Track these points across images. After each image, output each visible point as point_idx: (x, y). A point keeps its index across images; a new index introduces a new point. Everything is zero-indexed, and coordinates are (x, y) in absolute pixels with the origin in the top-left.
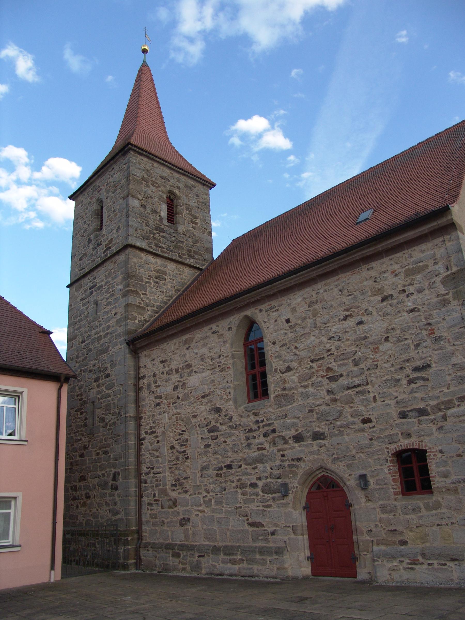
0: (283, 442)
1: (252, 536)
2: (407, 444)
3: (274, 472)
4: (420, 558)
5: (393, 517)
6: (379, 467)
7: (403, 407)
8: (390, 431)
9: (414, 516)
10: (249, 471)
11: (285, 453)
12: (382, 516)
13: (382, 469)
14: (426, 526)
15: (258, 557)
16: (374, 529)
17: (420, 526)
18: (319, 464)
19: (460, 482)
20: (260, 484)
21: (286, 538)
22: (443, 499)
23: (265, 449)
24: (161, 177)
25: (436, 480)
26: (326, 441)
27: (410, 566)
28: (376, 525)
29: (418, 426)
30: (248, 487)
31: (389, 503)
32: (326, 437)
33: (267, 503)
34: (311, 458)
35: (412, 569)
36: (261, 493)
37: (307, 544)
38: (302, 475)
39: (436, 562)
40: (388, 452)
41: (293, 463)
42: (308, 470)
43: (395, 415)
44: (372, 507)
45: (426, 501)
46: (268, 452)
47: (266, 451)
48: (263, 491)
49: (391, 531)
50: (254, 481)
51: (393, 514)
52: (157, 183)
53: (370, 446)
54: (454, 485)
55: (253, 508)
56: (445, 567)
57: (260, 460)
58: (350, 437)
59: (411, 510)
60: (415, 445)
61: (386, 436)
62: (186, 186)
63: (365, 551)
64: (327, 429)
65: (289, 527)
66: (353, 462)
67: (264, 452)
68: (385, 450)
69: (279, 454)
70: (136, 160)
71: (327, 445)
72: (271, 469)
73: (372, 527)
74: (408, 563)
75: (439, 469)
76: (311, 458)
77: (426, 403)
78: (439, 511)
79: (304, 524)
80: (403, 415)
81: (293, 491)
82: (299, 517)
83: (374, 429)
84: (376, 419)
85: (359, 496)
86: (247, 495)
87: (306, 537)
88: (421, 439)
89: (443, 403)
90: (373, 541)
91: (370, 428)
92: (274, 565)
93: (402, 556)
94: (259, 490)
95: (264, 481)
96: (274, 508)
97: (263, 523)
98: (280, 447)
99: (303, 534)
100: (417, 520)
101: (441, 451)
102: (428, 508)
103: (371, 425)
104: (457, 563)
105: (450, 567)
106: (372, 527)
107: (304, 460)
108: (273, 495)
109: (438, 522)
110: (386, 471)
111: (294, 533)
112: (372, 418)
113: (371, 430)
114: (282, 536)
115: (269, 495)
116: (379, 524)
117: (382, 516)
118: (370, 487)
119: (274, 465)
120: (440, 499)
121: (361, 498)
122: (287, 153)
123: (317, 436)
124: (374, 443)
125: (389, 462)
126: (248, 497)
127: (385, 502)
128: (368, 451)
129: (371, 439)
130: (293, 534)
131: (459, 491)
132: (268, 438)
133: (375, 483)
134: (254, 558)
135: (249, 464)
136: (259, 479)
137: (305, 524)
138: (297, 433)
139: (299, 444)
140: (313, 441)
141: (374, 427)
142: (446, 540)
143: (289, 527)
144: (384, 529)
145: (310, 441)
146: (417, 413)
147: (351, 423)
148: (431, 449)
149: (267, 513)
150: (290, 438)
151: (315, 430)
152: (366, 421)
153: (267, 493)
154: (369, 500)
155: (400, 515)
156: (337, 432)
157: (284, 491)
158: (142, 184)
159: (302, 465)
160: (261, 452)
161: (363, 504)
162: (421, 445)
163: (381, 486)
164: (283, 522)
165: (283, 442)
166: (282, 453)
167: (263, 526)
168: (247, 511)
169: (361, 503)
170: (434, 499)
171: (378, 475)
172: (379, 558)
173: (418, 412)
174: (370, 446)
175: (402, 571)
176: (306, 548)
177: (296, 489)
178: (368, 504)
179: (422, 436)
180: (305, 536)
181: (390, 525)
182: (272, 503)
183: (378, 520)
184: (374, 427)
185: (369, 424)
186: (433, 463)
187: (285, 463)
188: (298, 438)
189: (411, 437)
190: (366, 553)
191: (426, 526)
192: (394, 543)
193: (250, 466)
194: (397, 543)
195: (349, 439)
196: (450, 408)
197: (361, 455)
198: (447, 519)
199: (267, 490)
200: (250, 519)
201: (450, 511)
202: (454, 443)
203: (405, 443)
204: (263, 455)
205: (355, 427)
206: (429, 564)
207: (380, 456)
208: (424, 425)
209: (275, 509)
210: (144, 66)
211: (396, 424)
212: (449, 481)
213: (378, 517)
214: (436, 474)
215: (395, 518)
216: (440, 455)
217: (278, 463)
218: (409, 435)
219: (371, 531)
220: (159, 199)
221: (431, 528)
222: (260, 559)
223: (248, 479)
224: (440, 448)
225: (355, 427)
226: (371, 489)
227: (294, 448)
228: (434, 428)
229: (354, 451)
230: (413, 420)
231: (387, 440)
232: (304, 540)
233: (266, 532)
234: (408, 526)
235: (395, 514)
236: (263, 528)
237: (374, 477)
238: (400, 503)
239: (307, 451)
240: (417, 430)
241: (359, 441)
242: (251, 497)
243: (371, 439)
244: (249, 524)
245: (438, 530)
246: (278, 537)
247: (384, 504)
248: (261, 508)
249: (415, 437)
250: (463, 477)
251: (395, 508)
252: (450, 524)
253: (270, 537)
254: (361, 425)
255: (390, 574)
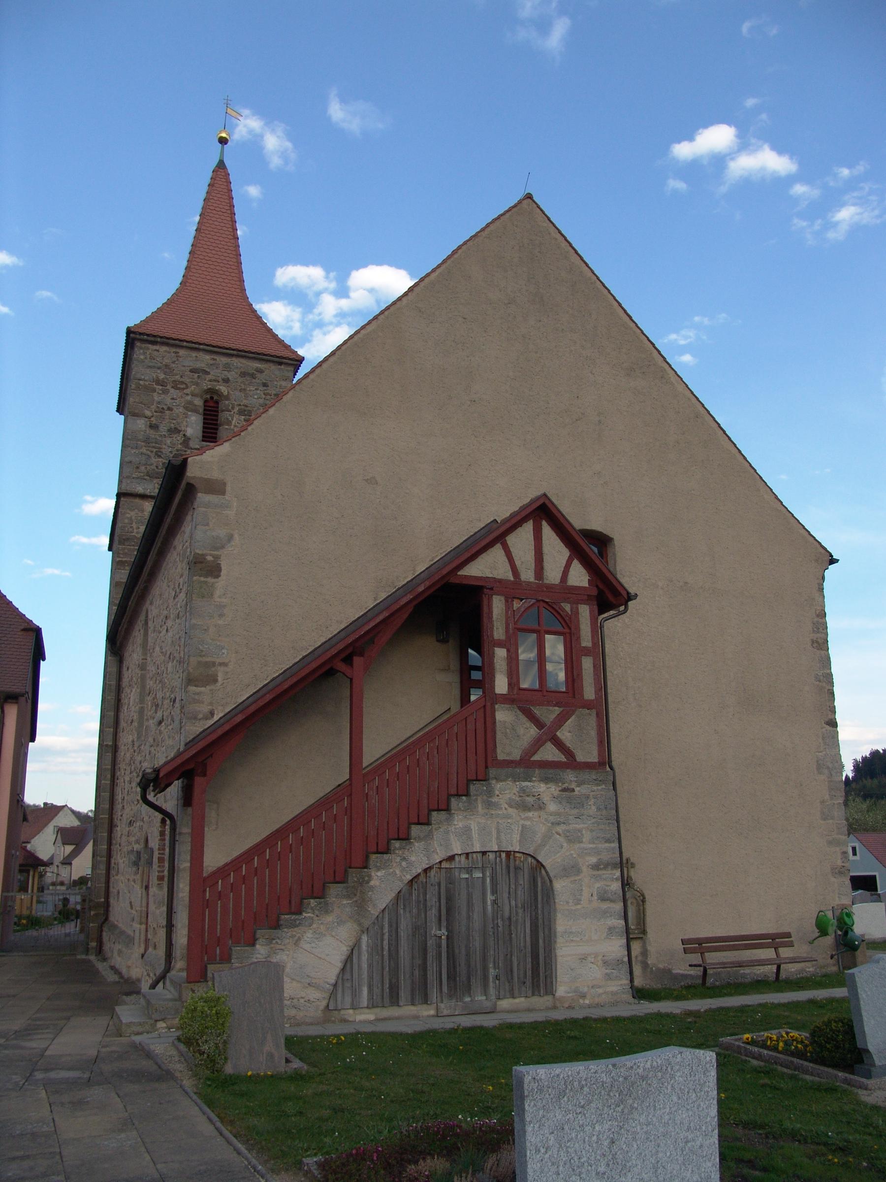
24: (191, 371)
52: (182, 383)
62: (243, 374)
70: (144, 353)
122: (790, 180)
158: (154, 390)
210: (221, 166)
220: (186, 408)
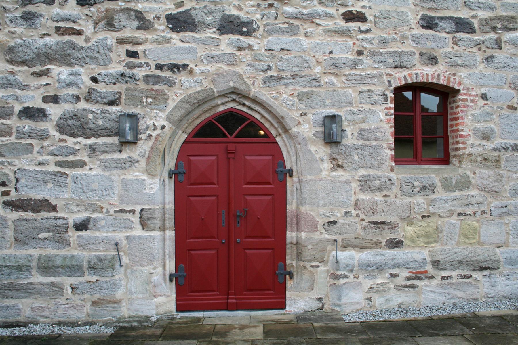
0: (136, 23)
1: (16, 230)
2: (427, 75)
3: (101, 88)
4: (429, 268)
5: (382, 199)
6: (368, 107)
7: (429, 9)
8: (399, 44)
9: (421, 200)
10: (20, 78)
11: (139, 49)
12: (362, 196)
13: (373, 112)
14: (440, 216)
15: (37, 278)
16: (340, 221)
17: (429, 216)
18: (231, 84)
19: (506, 149)
20: (55, 111)
21: (120, 236)
22: (475, 174)
23: (79, 33)
25: (469, 142)
26: (253, 39)
27: (409, 283)
28: (347, 213)
29: (453, 48)
30: (15, 117)
31: (379, 173)
32: (255, 30)
33: (71, 158)
34: (212, 68)
35: (413, 287)
36: (54, 133)
37: (170, 247)
38: (181, 101)
39: (454, 274)
40: (389, 82)
41: (158, 73)
42: (198, 92)
43: (414, 19)
44: (344, 179)
45: (446, 175)
46: (88, 40)
47: (83, 37)
48: (61, 128)
49: (376, 223)
50: (38, 103)
51: (385, 193)
53: (355, 65)
54: (496, 154)
55: (27, 168)
56: (469, 280)
57: (63, 56)
58: (311, 41)
59: (418, 189)
60: (442, 78)
61: (389, 53)
63: (315, 260)
64: (259, 16)
65: (133, 212)
66: (314, 89)
67: (74, 38)
68: (385, 79)
69: (122, 49)
71: (256, 47)
72: (94, 80)
73: (339, 215)
74: (407, 277)
75: (478, 126)
76: (212, 68)
77: (472, 13)
78: (465, 192)
79: (167, 207)
80: (429, 23)
81: (150, 136)
82: (159, 192)
83: (369, 36)
84: (375, 17)
85: (318, 156)
86: (10, 134)
87: (170, 234)
88: (453, 70)
89: (500, 19)
90: (336, 241)
91: (361, 32)
92: (86, 296)
93: (397, 266)
94: (49, 127)
95: (68, 107)
96: (94, 170)
97: (53, 203)
98: (126, 33)
99: (163, 229)
100: (426, 206)
101: (484, 97)
102: (448, 186)
103: (364, 27)
104: (486, 272)
105: (476, 280)
106: (338, 215)
107: (191, 72)
108: (92, 141)
109: (460, 210)
110: (382, 116)
111: (144, 225)
112: (367, 13)
113: (362, 36)
114: (108, 231)
115: (80, 139)
116: (353, 211)
117: (362, 196)
118: (344, 142)
119: (104, 72)
120: (469, 173)
121: (322, 160)
123: (230, 26)
124: (365, 61)
125: (389, 100)
126: (13, 139)
127: (371, 172)
128: (350, 74)
129: (360, 53)
130: (140, 227)
131: (503, 163)
132: (92, 9)
133: (356, 134)
134: (25, 281)
135: (23, 63)
136: (55, 99)
137: (170, 206)
138: (180, 10)
139: (182, 34)
140: (221, 34)
141: (368, 31)
142: (468, 238)
143: (133, 212)
144: (362, 220)
145: (211, 33)
146: (453, 25)
147: (319, 14)
148: (468, 89)
149: (69, 178)
150: (158, 18)
151: (226, 12)
152: (351, 17)
153: (73, 135)
154: (339, 166)
155: (396, 197)
156: (282, 26)
157: (126, 133)
159: (182, 78)
160: (67, 38)
161: (324, 173)
162: (452, 79)
163: (367, 143)
164: (115, 200)
165: (136, 23)
166: (129, 47)
167: (54, 209)
168: (7, 175)
169: (321, 171)
170: (461, 171)
171: (364, 122)
172: (351, 271)
173: (457, 24)
174: (355, 65)
175: (393, 291)
176: (167, 257)
177: (159, 131)
178: (335, 174)
179: (456, 65)
180: (167, 232)
181: (375, 212)
182: (86, 159)
183: (353, 203)
184: (368, 31)
185: (358, 24)
186: (469, 113)
187: (136, 71)
188: (180, 23)
189: (436, 63)
190: (316, 264)
191: (440, 216)
192: (378, 245)
193: (25, 68)
194: (384, 244)
195: (311, 43)
196: (510, 29)
197: (334, 79)
198: (476, 205)
199: (74, 126)
200: (13, 193)
201: (482, 193)
202: (506, 86)
203: (425, 73)
204: (73, 46)
205: (330, 24)
206: (443, 278)
207: (372, 88)
208: (464, 48)
209: (93, 172)
211: (413, 36)
212: (489, 145)
213: (353, 198)
214: (470, 133)
215: (386, 201)
216: (481, 102)
217: (116, 69)
218: (433, 60)
219: (335, 222)
221: (447, 219)
222: (42, 284)
223: (17, 98)
224: (483, 90)
225: (330, 24)
226: (347, 146)
227: (168, 41)
228: (479, 57)
229: (318, 70)
230: (444, 35)
231: (390, 60)
232: (164, 239)
233: (61, 222)
234: (408, 215)
235: (387, 193)
236: (53, 214)
237: (355, 123)
238: (400, 176)
239: (201, 52)
240: (449, 53)
241: (331, 53)
242: (23, 141)
243: (360, 53)
244: (7, 204)
245: (459, 222)
246: (97, 234)
247: (369, 176)
248: (52, 168)
249: (445, 64)
250: (512, 142)
251: (389, 182)
252: (479, 213)
253: (73, 235)
254: (342, 23)
255: (369, 299)
